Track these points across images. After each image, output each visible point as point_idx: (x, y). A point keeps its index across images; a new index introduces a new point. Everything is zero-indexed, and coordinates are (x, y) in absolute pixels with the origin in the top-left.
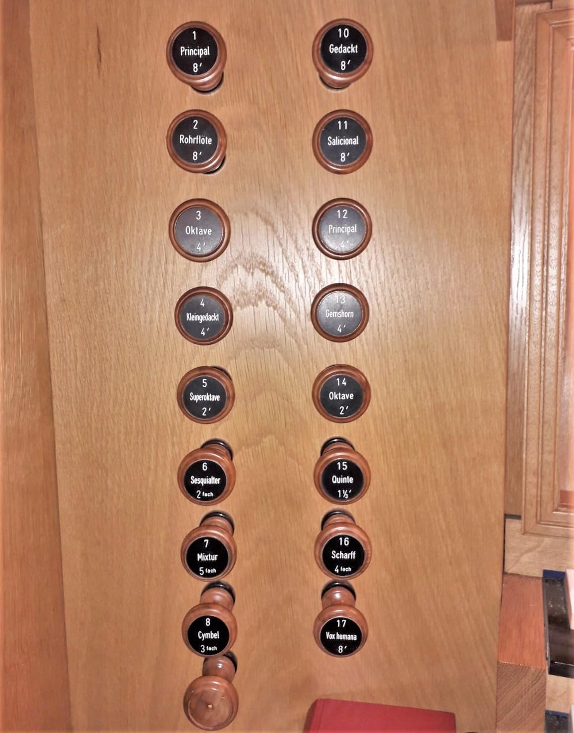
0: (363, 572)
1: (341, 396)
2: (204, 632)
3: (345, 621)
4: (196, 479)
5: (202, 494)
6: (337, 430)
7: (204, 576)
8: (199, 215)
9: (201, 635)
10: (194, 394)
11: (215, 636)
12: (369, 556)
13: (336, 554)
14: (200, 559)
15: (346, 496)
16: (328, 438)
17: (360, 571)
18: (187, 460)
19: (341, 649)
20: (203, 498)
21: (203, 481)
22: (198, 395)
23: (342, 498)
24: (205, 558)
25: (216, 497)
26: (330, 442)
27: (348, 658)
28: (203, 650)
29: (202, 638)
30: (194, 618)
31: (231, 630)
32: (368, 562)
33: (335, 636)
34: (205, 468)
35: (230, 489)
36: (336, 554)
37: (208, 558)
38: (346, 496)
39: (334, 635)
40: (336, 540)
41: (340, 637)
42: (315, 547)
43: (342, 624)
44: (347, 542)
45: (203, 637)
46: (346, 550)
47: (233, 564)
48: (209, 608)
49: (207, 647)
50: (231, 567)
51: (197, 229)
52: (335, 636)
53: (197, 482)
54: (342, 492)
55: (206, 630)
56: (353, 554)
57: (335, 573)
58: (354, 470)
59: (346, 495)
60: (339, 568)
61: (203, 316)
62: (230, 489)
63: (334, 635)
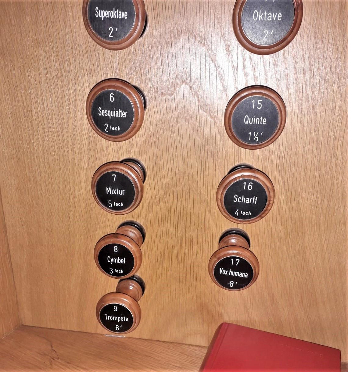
0: (263, 217)
1: (267, 16)
2: (113, 257)
3: (239, 260)
4: (103, 110)
5: (109, 127)
6: (247, 156)
7: (112, 208)
8: (112, 271)
9: (110, 260)
10: (101, 9)
11: (122, 261)
12: (271, 202)
13: (238, 198)
14: (109, 193)
15: (256, 139)
16: (237, 164)
17: (260, 216)
18: (96, 90)
19: (232, 284)
20: (111, 132)
21: (110, 114)
22: (103, 11)
23: (252, 141)
24: (113, 192)
25: (125, 131)
26: (230, 232)
27: (237, 293)
28: (111, 272)
29: (111, 262)
30: (103, 244)
31: (136, 257)
32: (269, 208)
33: (228, 273)
34: (112, 99)
35: (138, 125)
36: (238, 198)
37: (116, 192)
38: (256, 139)
39: (227, 272)
40: (240, 183)
41: (232, 273)
42: (219, 189)
43: (235, 262)
44: (250, 187)
45: (112, 261)
46: (249, 195)
47: (139, 200)
48: (117, 237)
49: (115, 270)
50: (137, 203)
51: (117, 12)
52: (228, 273)
53: (105, 114)
54: (252, 134)
55: (114, 256)
56: (255, 199)
57: (235, 216)
58: (259, 191)
59: (256, 138)
60: (239, 212)
61: (113, 108)
62: (138, 125)
63: (227, 272)
